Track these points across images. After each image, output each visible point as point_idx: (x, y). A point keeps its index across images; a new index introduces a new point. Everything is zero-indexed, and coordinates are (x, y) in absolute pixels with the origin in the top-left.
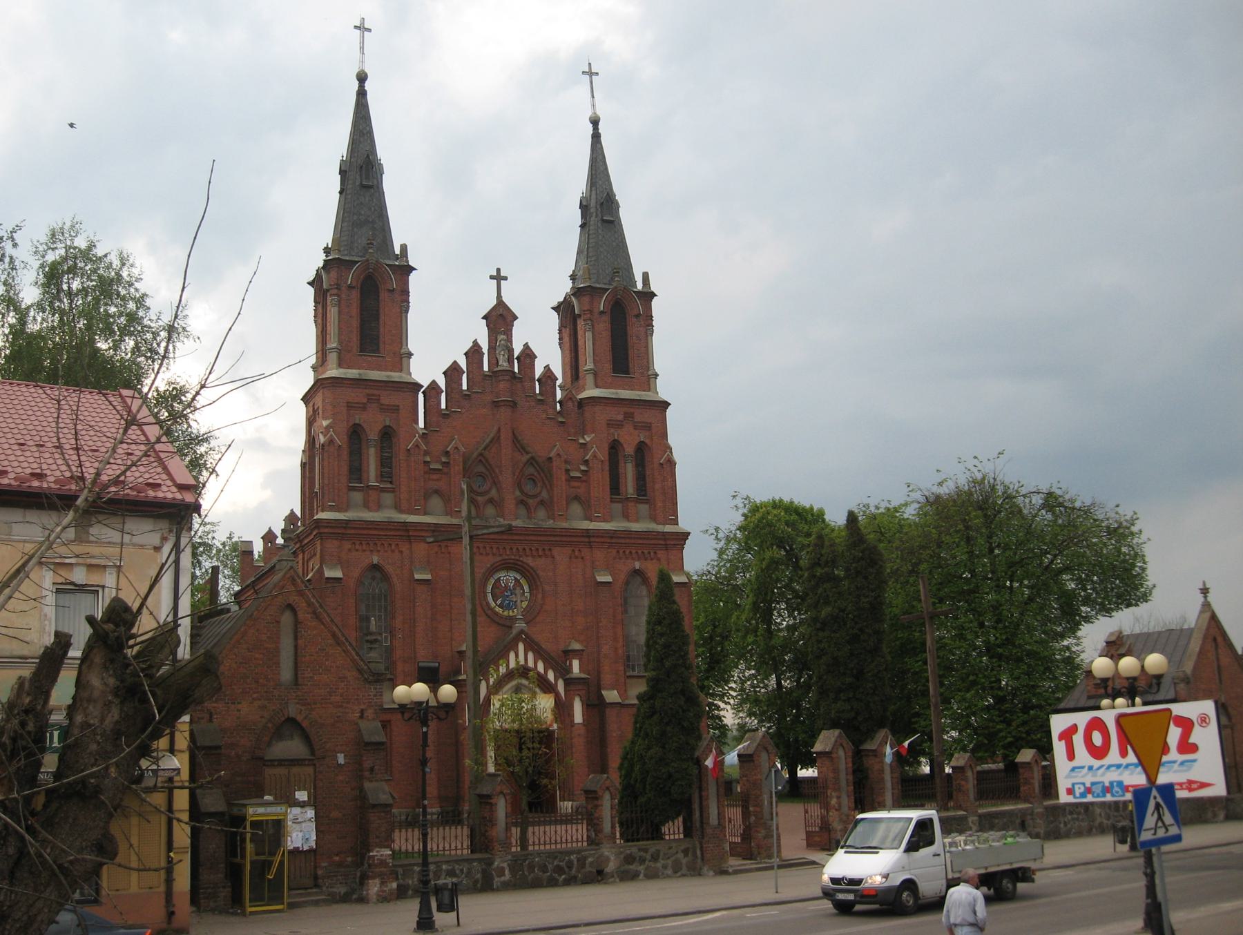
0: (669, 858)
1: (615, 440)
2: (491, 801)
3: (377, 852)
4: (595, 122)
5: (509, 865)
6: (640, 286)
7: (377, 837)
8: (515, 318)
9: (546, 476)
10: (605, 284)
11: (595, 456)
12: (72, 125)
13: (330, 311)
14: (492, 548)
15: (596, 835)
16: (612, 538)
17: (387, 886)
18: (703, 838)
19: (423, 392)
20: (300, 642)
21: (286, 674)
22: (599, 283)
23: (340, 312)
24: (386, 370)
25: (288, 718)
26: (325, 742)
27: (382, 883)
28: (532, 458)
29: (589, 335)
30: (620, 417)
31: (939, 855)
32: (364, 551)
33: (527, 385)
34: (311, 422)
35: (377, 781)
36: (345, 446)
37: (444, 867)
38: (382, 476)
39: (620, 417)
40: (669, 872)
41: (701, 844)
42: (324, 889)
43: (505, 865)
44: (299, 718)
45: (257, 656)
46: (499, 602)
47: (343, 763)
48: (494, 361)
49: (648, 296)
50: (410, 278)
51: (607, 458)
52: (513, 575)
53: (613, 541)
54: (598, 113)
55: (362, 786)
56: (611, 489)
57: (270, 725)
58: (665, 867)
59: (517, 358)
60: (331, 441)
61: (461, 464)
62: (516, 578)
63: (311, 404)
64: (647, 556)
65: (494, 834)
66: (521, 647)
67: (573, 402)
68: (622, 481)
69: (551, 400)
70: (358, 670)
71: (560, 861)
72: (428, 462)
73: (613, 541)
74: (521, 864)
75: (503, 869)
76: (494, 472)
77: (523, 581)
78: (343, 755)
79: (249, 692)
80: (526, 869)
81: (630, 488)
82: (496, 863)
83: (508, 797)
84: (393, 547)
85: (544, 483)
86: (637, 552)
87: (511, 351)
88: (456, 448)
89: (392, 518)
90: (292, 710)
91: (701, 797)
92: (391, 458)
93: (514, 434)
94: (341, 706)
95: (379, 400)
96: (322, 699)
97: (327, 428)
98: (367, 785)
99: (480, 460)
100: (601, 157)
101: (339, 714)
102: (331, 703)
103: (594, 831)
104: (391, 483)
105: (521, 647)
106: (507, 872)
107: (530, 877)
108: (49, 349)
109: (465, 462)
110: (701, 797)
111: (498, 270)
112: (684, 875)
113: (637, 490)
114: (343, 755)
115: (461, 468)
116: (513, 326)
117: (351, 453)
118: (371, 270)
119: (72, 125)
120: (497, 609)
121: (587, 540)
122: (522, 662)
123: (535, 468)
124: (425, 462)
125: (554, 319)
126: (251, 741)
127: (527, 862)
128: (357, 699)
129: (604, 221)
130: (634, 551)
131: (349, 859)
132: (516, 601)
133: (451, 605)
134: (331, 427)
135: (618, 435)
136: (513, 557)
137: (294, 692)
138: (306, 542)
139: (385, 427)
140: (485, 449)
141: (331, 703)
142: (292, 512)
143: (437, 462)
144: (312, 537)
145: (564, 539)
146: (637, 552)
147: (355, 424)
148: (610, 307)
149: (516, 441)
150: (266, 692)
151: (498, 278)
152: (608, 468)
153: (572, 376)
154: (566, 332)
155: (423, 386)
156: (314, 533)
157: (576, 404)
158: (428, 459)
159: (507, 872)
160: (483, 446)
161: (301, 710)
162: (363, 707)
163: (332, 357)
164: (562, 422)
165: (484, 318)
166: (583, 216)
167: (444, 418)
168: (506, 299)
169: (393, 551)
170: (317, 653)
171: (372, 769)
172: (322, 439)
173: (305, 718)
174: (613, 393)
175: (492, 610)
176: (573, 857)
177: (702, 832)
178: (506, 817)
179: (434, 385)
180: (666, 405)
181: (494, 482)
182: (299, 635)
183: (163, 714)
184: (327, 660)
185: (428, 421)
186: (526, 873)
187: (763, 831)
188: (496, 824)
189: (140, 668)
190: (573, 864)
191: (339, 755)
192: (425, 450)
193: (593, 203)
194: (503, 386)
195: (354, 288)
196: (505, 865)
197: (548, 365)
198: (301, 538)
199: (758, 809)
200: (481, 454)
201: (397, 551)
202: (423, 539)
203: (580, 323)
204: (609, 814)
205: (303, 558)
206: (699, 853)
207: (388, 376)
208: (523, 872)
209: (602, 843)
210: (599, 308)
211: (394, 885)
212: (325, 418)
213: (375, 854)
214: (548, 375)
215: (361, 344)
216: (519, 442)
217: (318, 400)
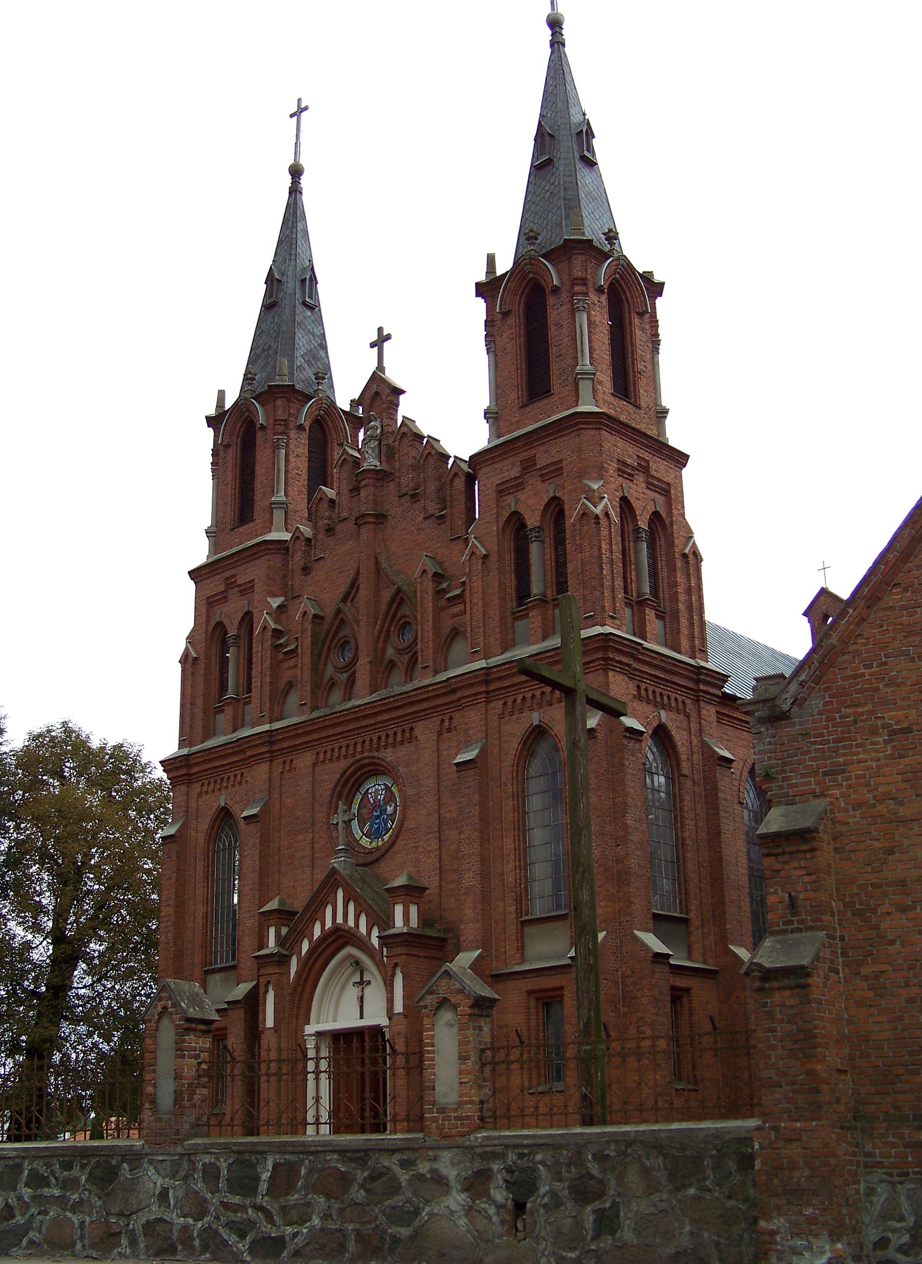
4: (296, 172)
8: (657, 289)
30: (515, 472)
31: (362, 1017)
32: (213, 791)
53: (492, 687)
66: (340, 894)
73: (492, 687)
118: (531, 276)
122: (340, 920)
132: (337, 824)
145: (425, 705)
166: (269, 294)
183: (44, 1114)
189: (261, 1152)
192: (275, 630)
202: (255, 759)
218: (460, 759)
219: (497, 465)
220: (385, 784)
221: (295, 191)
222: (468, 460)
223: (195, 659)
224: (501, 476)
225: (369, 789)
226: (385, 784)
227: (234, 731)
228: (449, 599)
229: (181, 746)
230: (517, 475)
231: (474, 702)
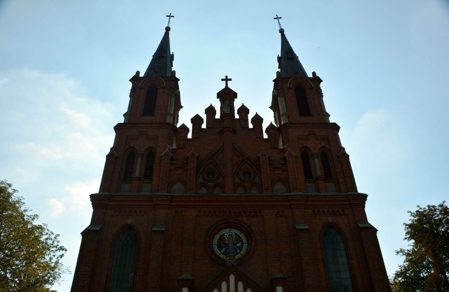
1: (304, 147)
4: (282, 31)
12: (418, 107)
30: (306, 134)
46: (223, 251)
52: (234, 231)
53: (308, 203)
54: (282, 28)
62: (236, 234)
66: (232, 278)
73: (308, 203)
77: (242, 236)
88: (193, 154)
100: (169, 46)
105: (232, 278)
108: (27, 227)
119: (418, 107)
120: (222, 256)
121: (287, 203)
136: (231, 218)
151: (227, 80)
218: (154, 229)
220: (235, 233)
221: (283, 36)
222: (166, 122)
223: (117, 157)
224: (299, 133)
225: (225, 233)
226: (235, 233)
227: (138, 192)
228: (176, 167)
229: (99, 192)
230: (307, 135)
231: (299, 207)
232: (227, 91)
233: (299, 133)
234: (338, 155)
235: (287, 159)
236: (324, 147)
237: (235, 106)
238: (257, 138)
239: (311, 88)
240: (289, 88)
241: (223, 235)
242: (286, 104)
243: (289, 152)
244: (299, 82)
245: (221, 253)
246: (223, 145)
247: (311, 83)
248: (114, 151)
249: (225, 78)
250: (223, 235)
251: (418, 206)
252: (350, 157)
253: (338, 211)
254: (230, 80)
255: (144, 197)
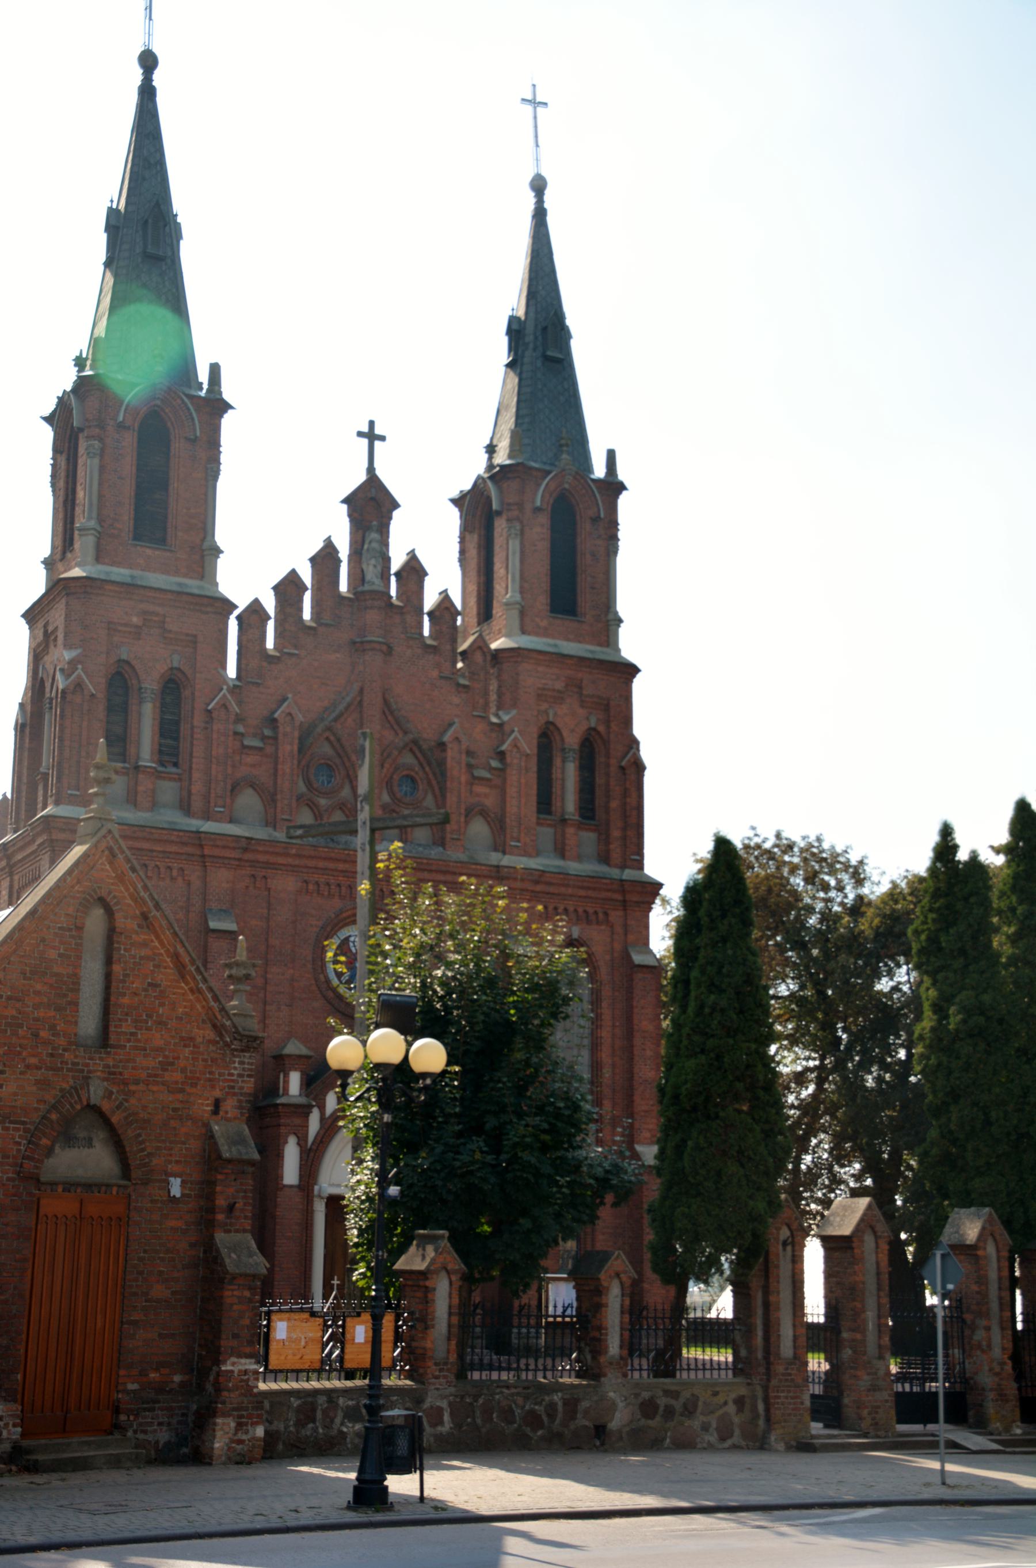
0: (712, 1412)
1: (548, 723)
2: (427, 1283)
3: (233, 1364)
5: (450, 1404)
6: (599, 471)
7: (235, 1336)
8: (395, 505)
9: (434, 774)
10: (545, 463)
11: (515, 745)
13: (85, 464)
14: (339, 885)
15: (594, 1358)
16: (537, 882)
17: (247, 1432)
18: (769, 1380)
19: (239, 618)
20: (117, 968)
21: (88, 1024)
22: (535, 461)
23: (102, 469)
24: (177, 573)
25: (88, 1105)
26: (150, 1155)
27: (240, 1426)
28: (415, 742)
29: (515, 545)
33: (409, 619)
34: (37, 656)
35: (237, 1231)
36: (100, 696)
37: (341, 1401)
38: (160, 752)
39: (559, 685)
40: (712, 1437)
41: (766, 1389)
42: (130, 1434)
43: (444, 1404)
44: (106, 1106)
45: (38, 987)
47: (178, 1195)
48: (357, 577)
49: (613, 487)
50: (223, 421)
51: (535, 751)
55: (212, 1237)
56: (539, 803)
57: (54, 1116)
58: (705, 1428)
59: (398, 574)
60: (79, 686)
61: (296, 741)
63: (40, 624)
64: (593, 918)
65: (428, 1345)
67: (484, 653)
68: (556, 789)
69: (448, 647)
70: (214, 1026)
71: (536, 1404)
72: (242, 735)
74: (471, 1404)
75: (440, 1410)
76: (349, 759)
78: (179, 1180)
79: (20, 1053)
80: (478, 1413)
81: (569, 802)
82: (429, 1400)
83: (454, 1278)
84: (175, 873)
85: (429, 783)
86: (576, 911)
87: (387, 560)
89: (175, 823)
90: (96, 1092)
91: (766, 1305)
92: (177, 723)
93: (386, 702)
94: (182, 1091)
95: (164, 622)
96: (149, 1075)
97: (73, 663)
98: (220, 1237)
99: (327, 739)
101: (177, 1105)
102: (163, 1084)
103: (591, 1352)
104: (176, 765)
106: (446, 1417)
107: (484, 1430)
109: (302, 740)
110: (766, 1305)
111: (372, 424)
112: (735, 1447)
113: (581, 808)
114: (179, 1180)
115: (296, 748)
116: (390, 518)
117: (110, 709)
123: (417, 758)
124: (236, 733)
125: (453, 517)
126: (19, 1144)
127: (481, 1401)
128: (210, 1080)
129: (547, 359)
130: (571, 909)
131: (177, 1378)
133: (266, 979)
134: (80, 662)
135: (555, 714)
137: (101, 1059)
138: (19, 857)
139: (172, 669)
140: (336, 720)
141: (163, 1084)
142: (4, 795)
143: (255, 735)
144: (34, 847)
146: (576, 911)
147: (119, 661)
148: (551, 501)
149: (389, 712)
150: (52, 1055)
151: (371, 436)
152: (535, 769)
153: (479, 614)
154: (473, 540)
155: (236, 607)
156: (39, 841)
157: (489, 658)
158: (241, 729)
159: (446, 1417)
160: (334, 715)
161: (112, 1093)
162: (217, 1093)
163: (84, 544)
164: (465, 686)
165: (346, 501)
167: (270, 663)
168: (380, 473)
169: (173, 879)
170: (145, 990)
171: (231, 1208)
172: (61, 683)
173: (118, 1107)
174: (550, 645)
175: (334, 990)
176: (557, 1398)
177: (768, 1369)
178: (450, 1314)
179: (256, 608)
180: (632, 670)
181: (348, 776)
182: (115, 957)
184: (162, 1005)
185: (243, 666)
186: (479, 1421)
187: (866, 1377)
188: (433, 1326)
190: (556, 1410)
191: (172, 1179)
192: (237, 714)
193: (530, 329)
194: (373, 616)
195: (128, 428)
196: (444, 1404)
197: (446, 591)
198: (10, 851)
199: (859, 1336)
200: (329, 729)
201: (180, 879)
203: (500, 525)
204: (617, 1321)
205: (11, 887)
206: (761, 1407)
207: (180, 584)
208: (474, 1419)
209: (605, 1375)
210: (533, 502)
211: (260, 1431)
212: (68, 646)
213: (229, 1368)
214: (445, 600)
215: (136, 528)
216: (392, 713)
217: (57, 617)
219: (540, 669)
232: (373, 490)
233: (543, 681)
234: (623, 763)
235: (508, 760)
236: (594, 729)
237: (391, 554)
238: (442, 678)
239: (596, 520)
240: (538, 510)
241: (347, 939)
242: (522, 562)
243: (516, 738)
244: (566, 486)
245: (341, 982)
246: (361, 691)
247: (598, 495)
248: (84, 677)
249: (366, 429)
250: (347, 939)
251: (753, 828)
252: (646, 773)
253: (596, 913)
254: (382, 438)
255: (181, 834)
